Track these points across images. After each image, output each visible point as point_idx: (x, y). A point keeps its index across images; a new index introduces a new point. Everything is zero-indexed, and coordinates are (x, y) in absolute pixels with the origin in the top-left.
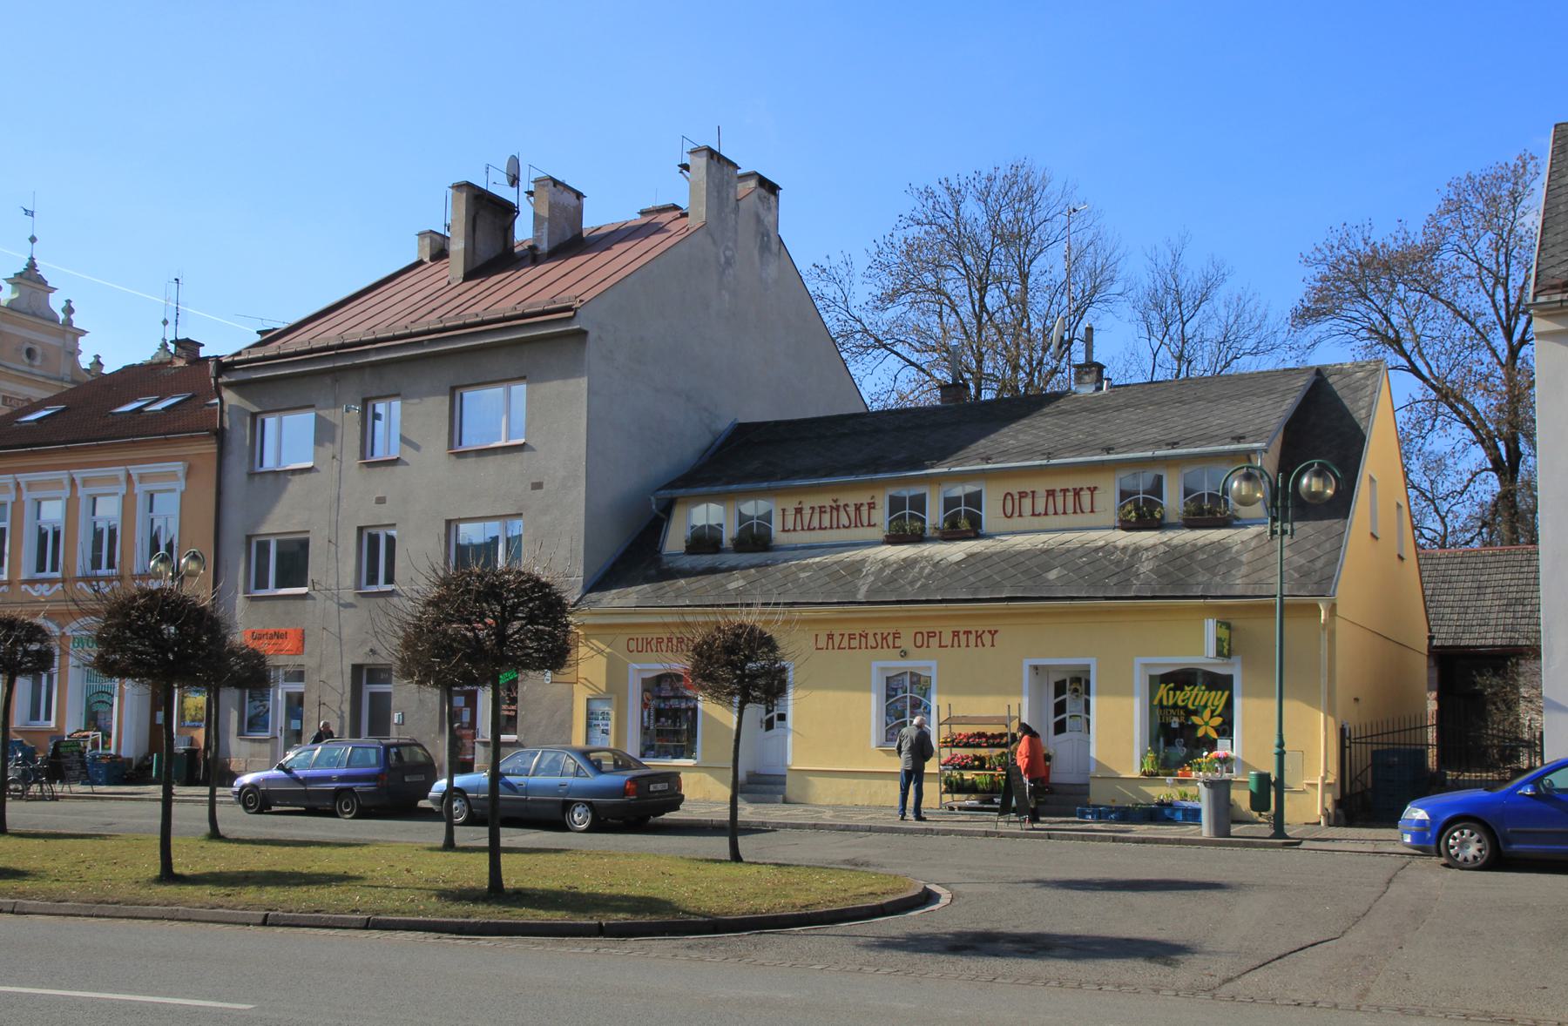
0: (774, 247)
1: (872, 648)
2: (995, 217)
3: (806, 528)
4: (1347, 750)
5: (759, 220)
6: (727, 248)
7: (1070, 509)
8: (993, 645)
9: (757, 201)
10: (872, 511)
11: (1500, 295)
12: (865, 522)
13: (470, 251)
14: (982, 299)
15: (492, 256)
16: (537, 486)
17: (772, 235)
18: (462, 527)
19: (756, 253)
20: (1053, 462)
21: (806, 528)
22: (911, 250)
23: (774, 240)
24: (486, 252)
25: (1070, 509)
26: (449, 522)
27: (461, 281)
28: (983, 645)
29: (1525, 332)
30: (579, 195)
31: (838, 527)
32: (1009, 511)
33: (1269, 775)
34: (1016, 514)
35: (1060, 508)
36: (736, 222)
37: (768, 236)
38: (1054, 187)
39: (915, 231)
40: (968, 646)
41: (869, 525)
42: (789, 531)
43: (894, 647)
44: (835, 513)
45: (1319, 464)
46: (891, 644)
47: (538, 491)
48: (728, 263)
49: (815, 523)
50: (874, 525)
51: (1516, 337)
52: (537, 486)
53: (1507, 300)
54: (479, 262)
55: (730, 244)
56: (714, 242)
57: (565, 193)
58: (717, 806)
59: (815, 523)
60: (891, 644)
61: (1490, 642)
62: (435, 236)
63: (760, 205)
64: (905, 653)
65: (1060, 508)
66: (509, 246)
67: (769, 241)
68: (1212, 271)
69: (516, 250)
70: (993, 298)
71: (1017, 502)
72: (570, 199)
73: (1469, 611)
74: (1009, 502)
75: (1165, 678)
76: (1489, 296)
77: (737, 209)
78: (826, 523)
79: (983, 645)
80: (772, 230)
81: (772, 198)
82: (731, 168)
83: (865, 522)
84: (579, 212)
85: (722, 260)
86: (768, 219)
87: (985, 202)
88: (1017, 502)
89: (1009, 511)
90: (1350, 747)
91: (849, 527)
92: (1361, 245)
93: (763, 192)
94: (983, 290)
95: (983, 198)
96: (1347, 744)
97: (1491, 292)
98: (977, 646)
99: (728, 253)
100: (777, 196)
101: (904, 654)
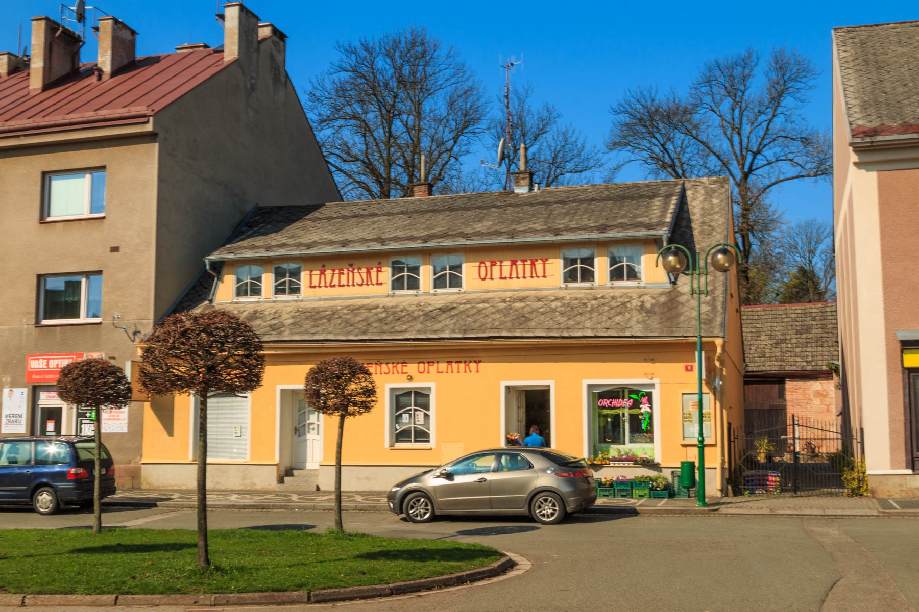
0: (283, 79)
1: (385, 373)
2: (398, 69)
3: (328, 284)
4: (732, 443)
5: (272, 58)
6: (252, 78)
7: (528, 274)
8: (478, 372)
9: (272, 45)
10: (380, 273)
11: (736, 138)
12: (374, 281)
13: (48, 69)
14: (390, 128)
15: (64, 74)
16: (115, 249)
17: (282, 70)
18: (49, 280)
19: (271, 83)
20: (516, 240)
21: (328, 284)
22: (341, 90)
23: (283, 74)
24: (61, 68)
25: (528, 274)
26: (39, 277)
27: (40, 91)
28: (470, 371)
29: (752, 163)
30: (133, 33)
31: (353, 285)
32: (483, 276)
33: (693, 463)
34: (489, 276)
35: (521, 275)
36: (258, 59)
37: (279, 71)
38: (442, 52)
39: (345, 76)
40: (459, 372)
41: (378, 284)
42: (505, 278)
43: (403, 373)
44: (351, 275)
45: (676, 248)
46: (400, 371)
47: (116, 253)
48: (253, 88)
49: (335, 282)
50: (381, 284)
51: (746, 169)
52: (115, 249)
53: (741, 143)
54: (53, 79)
55: (254, 75)
56: (244, 73)
57: (123, 30)
58: (152, 492)
59: (335, 282)
60: (400, 371)
61: (768, 368)
62: (13, 58)
63: (273, 48)
64: (411, 377)
65: (521, 275)
66: (76, 67)
67: (279, 74)
68: (545, 114)
69: (81, 69)
70: (398, 126)
71: (489, 268)
72: (127, 35)
73: (752, 348)
74: (483, 269)
75: (602, 396)
76: (728, 139)
77: (258, 50)
78: (344, 281)
79: (470, 371)
80: (281, 66)
81: (282, 43)
82: (255, 20)
83: (374, 281)
84: (133, 44)
85: (249, 86)
86: (279, 58)
87: (392, 59)
88: (489, 268)
89: (483, 276)
90: (734, 442)
91: (361, 285)
92: (649, 103)
93: (276, 39)
94: (390, 124)
95: (389, 55)
96: (732, 439)
97: (729, 136)
98: (465, 372)
99: (253, 81)
100: (284, 42)
101: (410, 379)
